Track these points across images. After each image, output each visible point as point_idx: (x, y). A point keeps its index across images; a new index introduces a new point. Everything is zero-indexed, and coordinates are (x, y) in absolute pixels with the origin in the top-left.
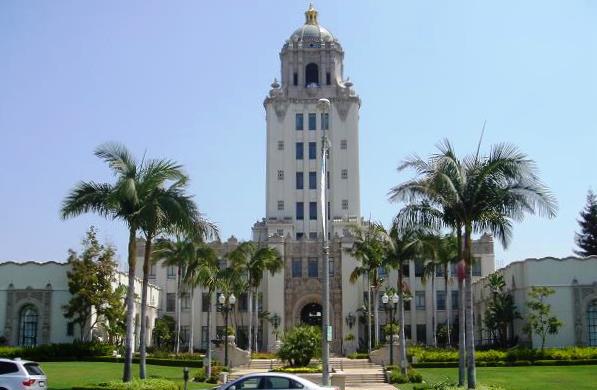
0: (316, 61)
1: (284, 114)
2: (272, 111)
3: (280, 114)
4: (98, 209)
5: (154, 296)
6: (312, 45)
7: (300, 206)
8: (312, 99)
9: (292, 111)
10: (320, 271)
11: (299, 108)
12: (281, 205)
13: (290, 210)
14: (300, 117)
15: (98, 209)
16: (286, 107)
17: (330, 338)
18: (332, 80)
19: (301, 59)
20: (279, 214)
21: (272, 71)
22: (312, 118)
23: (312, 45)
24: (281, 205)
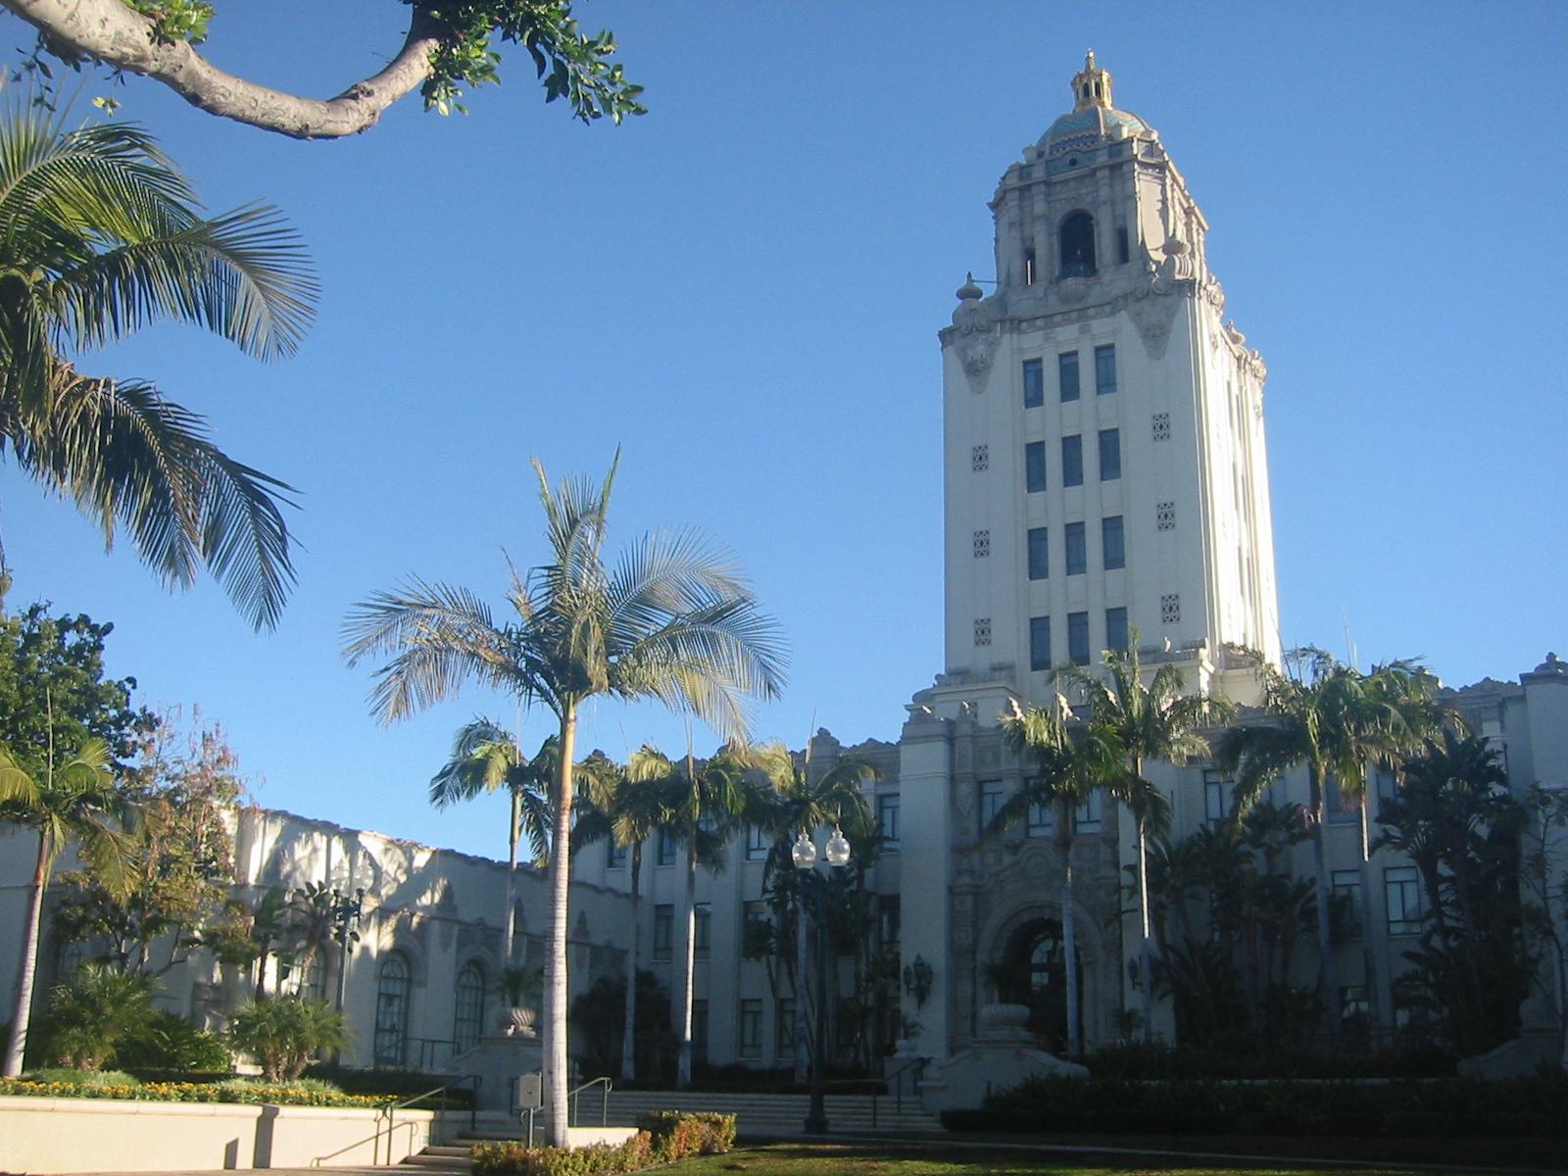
0: (1083, 205)
1: (988, 368)
2: (957, 366)
3: (975, 370)
4: (129, 502)
5: (37, 199)
6: (1073, 163)
7: (1039, 628)
8: (1079, 311)
9: (1007, 354)
10: (236, 320)
11: (1032, 343)
12: (982, 632)
13: (1011, 644)
14: (1032, 369)
15: (129, 502)
16: (992, 345)
17: (1266, 1081)
18: (1133, 253)
19: (1040, 207)
20: (982, 659)
21: (974, 252)
22: (1068, 365)
23: (1073, 163)
24: (982, 632)
